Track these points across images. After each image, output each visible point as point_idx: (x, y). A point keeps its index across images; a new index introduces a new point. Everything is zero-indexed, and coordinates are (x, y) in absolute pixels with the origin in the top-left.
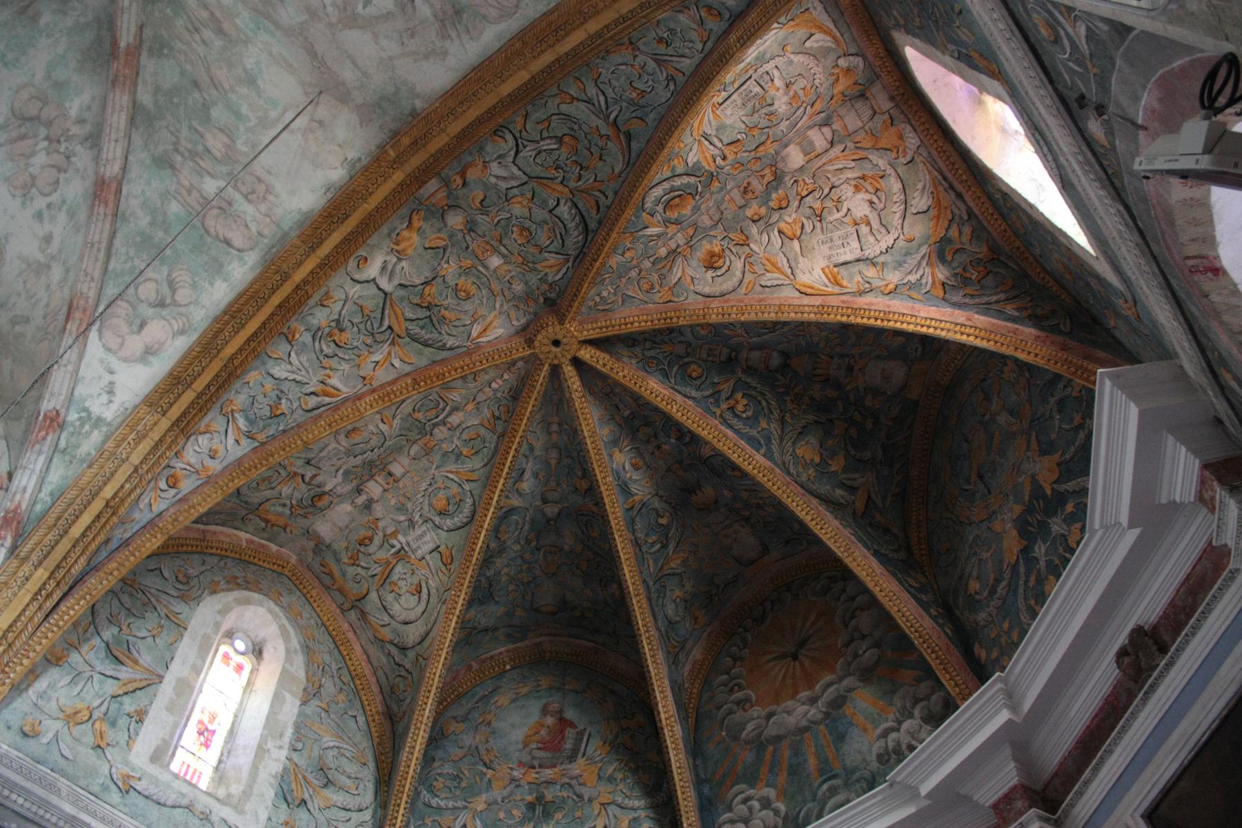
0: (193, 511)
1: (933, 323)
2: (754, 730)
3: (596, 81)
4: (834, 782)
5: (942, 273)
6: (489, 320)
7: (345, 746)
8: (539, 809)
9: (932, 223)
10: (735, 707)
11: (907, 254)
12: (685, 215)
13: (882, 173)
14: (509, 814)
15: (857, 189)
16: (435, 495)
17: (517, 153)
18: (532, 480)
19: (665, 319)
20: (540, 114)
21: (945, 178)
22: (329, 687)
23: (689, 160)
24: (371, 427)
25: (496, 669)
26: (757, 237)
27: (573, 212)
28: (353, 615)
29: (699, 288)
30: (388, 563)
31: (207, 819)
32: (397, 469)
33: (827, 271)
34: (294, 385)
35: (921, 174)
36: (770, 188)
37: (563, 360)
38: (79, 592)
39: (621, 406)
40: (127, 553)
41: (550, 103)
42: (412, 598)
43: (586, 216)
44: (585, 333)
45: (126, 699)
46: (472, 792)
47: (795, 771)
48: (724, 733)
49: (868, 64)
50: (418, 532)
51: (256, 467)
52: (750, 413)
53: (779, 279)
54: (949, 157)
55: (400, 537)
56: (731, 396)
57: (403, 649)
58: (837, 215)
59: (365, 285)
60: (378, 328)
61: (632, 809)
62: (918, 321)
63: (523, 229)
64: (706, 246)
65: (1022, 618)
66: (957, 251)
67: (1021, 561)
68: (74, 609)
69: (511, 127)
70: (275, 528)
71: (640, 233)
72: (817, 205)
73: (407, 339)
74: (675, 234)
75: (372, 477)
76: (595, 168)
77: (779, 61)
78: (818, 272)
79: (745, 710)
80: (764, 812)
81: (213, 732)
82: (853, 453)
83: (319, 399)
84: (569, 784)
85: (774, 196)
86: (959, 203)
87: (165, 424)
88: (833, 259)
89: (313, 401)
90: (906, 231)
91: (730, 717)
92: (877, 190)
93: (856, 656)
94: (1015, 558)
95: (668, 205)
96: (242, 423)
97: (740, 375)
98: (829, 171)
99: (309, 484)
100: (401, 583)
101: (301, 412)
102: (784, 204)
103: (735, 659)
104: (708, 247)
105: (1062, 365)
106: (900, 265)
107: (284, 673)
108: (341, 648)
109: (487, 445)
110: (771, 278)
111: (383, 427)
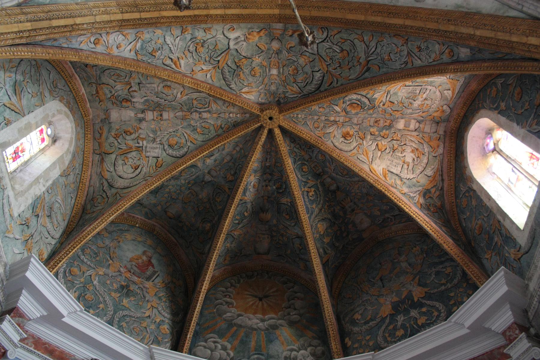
0: (96, 60)
1: (416, 214)
2: (230, 317)
3: (379, 42)
4: (261, 356)
5: (422, 201)
6: (253, 90)
7: (63, 207)
8: (125, 291)
9: (428, 182)
10: (224, 303)
11: (414, 186)
12: (352, 113)
13: (424, 153)
14: (112, 284)
15: (413, 151)
16: (173, 137)
17: (322, 42)
18: (213, 161)
19: (316, 142)
20: (345, 36)
21: (442, 171)
22: (71, 178)
23: (375, 96)
24: (175, 91)
25: (133, 223)
26: (368, 140)
27: (320, 78)
28: (97, 157)
29: (334, 141)
30: (131, 148)
31: (3, 190)
32: (165, 115)
33: (384, 170)
34: (168, 49)
35: (435, 163)
36: (384, 127)
37: (268, 126)
38: (30, 48)
39: (268, 160)
40: (60, 52)
41: (352, 36)
42: (131, 169)
43: (323, 84)
44: (284, 123)
45: (8, 111)
46: (100, 264)
47: (243, 342)
48: (215, 310)
49: (450, 115)
50: (154, 145)
51: (131, 66)
52: (312, 199)
53: (365, 160)
54: (451, 165)
55: (145, 142)
56: (310, 187)
57: (111, 186)
58: (400, 155)
59: (225, 38)
60: (215, 58)
61: (163, 316)
62: (411, 210)
63: (296, 69)
64: (348, 129)
65: (378, 338)
66: (430, 197)
67: (388, 318)
68: (24, 53)
69: (330, 31)
70: (97, 98)
71: (333, 106)
72: (396, 146)
73: (220, 71)
74: (341, 116)
75: (153, 110)
76: (344, 70)
77: (433, 89)
78: (380, 168)
79: (228, 307)
80: (222, 351)
81: (20, 157)
82: (334, 240)
83: (172, 63)
84: (142, 289)
85: (384, 131)
86: (441, 183)
87: (119, 17)
88: (389, 168)
89: (168, 62)
90: (419, 177)
91: (220, 305)
92: (418, 157)
93: (289, 314)
94: (386, 316)
95: (351, 105)
96: (139, 45)
97: (318, 183)
98: (408, 138)
99: (129, 92)
100: (131, 160)
101: (161, 62)
102: (385, 137)
103: (232, 285)
104: (349, 130)
105: (460, 259)
106: (410, 187)
107: (62, 157)
108: (84, 166)
109: (209, 134)
110: (362, 157)
111: (179, 95)
